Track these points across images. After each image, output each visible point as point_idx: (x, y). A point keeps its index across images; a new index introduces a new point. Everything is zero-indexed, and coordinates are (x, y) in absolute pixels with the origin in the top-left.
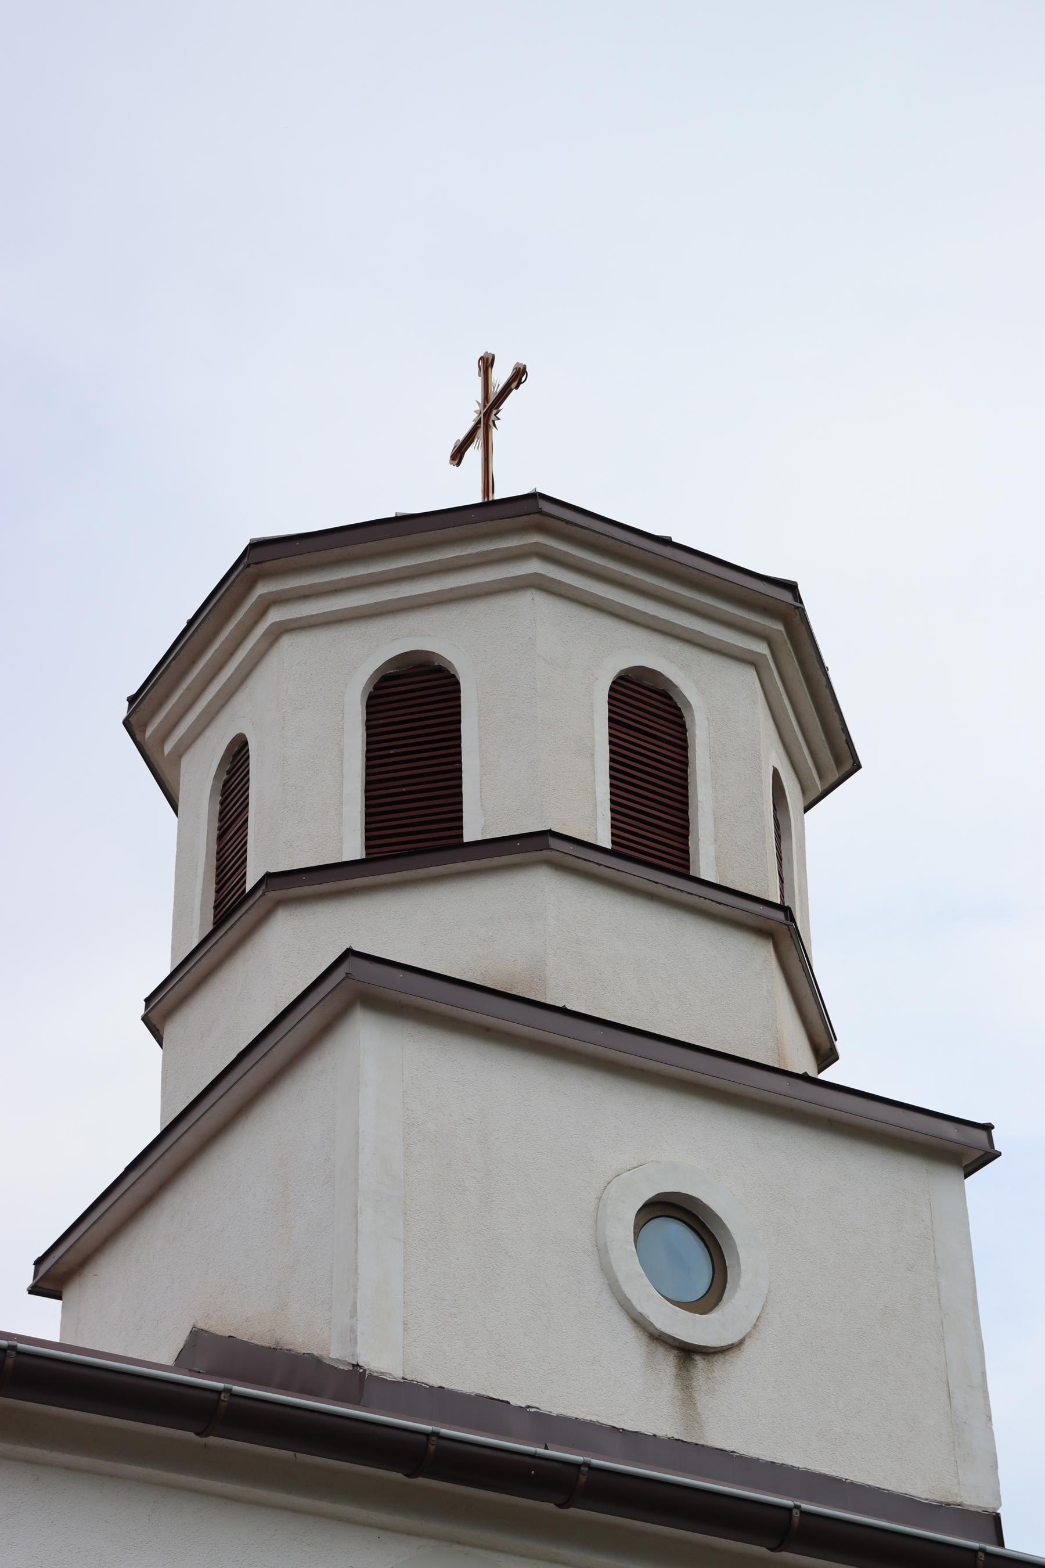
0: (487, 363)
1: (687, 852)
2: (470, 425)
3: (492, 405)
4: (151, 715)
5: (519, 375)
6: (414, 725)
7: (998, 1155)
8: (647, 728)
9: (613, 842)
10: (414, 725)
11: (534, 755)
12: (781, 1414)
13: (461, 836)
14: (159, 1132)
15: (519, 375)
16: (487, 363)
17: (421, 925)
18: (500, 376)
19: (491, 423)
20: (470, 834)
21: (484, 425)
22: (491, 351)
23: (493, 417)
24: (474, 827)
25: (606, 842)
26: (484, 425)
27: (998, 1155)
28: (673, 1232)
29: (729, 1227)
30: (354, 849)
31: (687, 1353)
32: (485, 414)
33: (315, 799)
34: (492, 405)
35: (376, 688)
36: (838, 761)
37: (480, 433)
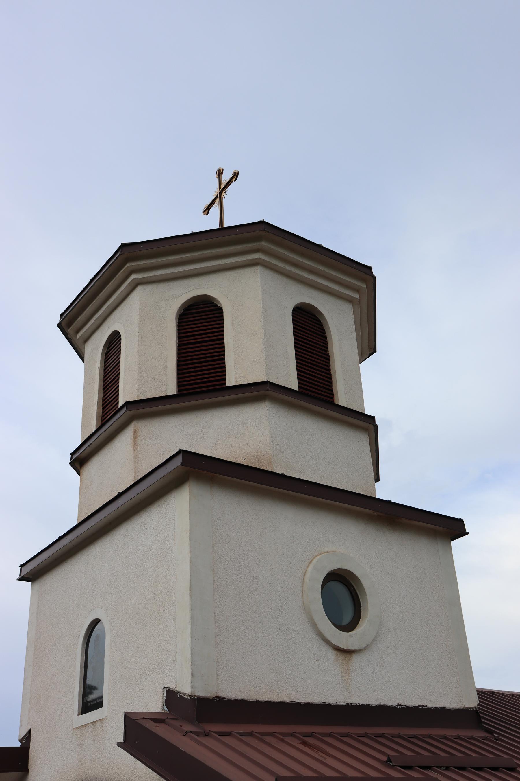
0: (220, 172)
1: (332, 391)
2: (231, 176)
3: (223, 189)
4: (74, 323)
5: (236, 175)
6: (200, 330)
7: (467, 533)
8: (309, 332)
9: (299, 387)
10: (200, 330)
11: (256, 344)
12: (385, 676)
13: (225, 384)
14: (76, 524)
15: (236, 175)
16: (220, 172)
17: (216, 433)
18: (226, 177)
19: (222, 196)
20: (230, 381)
21: (220, 196)
22: (221, 167)
23: (223, 194)
24: (232, 379)
25: (296, 387)
26: (220, 196)
27: (467, 533)
28: (339, 588)
29: (363, 583)
30: (172, 389)
31: (347, 652)
32: (220, 193)
33: (151, 367)
34: (223, 189)
35: (185, 310)
36: (370, 349)
37: (218, 200)
